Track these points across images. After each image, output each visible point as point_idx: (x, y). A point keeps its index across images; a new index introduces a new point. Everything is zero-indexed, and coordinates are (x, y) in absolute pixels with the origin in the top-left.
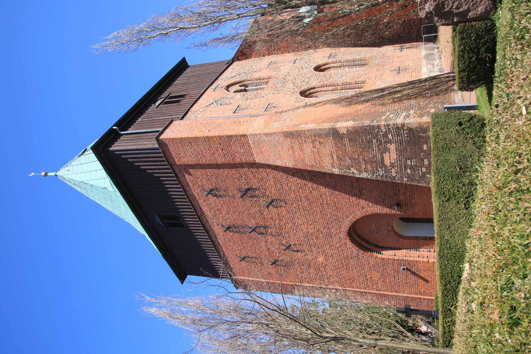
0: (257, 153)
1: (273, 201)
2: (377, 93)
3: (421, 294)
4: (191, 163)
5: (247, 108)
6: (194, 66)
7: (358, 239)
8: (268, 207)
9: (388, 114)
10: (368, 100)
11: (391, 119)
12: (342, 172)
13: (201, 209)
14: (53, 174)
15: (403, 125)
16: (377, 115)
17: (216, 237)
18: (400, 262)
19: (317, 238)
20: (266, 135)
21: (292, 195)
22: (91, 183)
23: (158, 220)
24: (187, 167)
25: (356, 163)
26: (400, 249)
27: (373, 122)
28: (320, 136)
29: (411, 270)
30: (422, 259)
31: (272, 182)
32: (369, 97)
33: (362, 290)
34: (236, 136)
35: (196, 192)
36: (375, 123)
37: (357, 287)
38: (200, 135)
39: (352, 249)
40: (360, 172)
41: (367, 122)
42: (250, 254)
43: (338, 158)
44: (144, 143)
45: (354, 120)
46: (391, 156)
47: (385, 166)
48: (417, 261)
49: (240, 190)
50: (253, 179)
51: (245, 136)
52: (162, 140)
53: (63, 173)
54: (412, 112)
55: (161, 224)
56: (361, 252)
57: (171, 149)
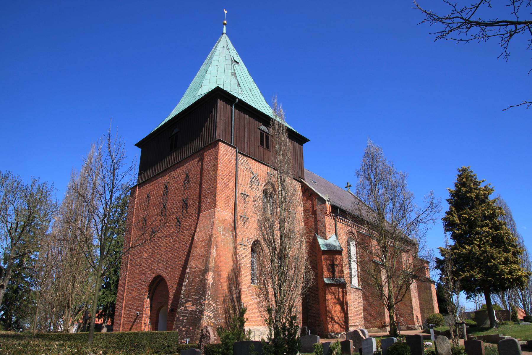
0: (205, 214)
1: (180, 222)
2: (237, 297)
3: (123, 325)
4: (205, 164)
5: (245, 202)
6: (301, 150)
7: (156, 282)
8: (176, 218)
9: (215, 305)
10: (231, 292)
11: (209, 307)
12: (187, 274)
13: (179, 167)
14: (225, 31)
15: (203, 315)
16: (214, 298)
17: (162, 177)
18: (142, 311)
19: (158, 253)
20: (213, 222)
21: (182, 237)
22: (209, 70)
23: (176, 130)
24: (202, 160)
25: (189, 285)
26: (151, 311)
27: (209, 295)
28: (207, 260)
29: (137, 319)
30: (143, 326)
31: (190, 223)
32: (234, 292)
33: (126, 284)
34: (215, 200)
35: (188, 165)
36: (207, 297)
37: (128, 280)
38: (219, 173)
39: (150, 277)
41: (209, 292)
42: (151, 202)
43: (194, 271)
44: (222, 126)
45: (213, 283)
46: (190, 307)
47: (186, 303)
48: (141, 323)
49: (187, 199)
50: (192, 210)
51: (215, 206)
52: (218, 144)
53: (225, 40)
54: (213, 320)
55: (173, 133)
56: (148, 284)
57: (212, 150)
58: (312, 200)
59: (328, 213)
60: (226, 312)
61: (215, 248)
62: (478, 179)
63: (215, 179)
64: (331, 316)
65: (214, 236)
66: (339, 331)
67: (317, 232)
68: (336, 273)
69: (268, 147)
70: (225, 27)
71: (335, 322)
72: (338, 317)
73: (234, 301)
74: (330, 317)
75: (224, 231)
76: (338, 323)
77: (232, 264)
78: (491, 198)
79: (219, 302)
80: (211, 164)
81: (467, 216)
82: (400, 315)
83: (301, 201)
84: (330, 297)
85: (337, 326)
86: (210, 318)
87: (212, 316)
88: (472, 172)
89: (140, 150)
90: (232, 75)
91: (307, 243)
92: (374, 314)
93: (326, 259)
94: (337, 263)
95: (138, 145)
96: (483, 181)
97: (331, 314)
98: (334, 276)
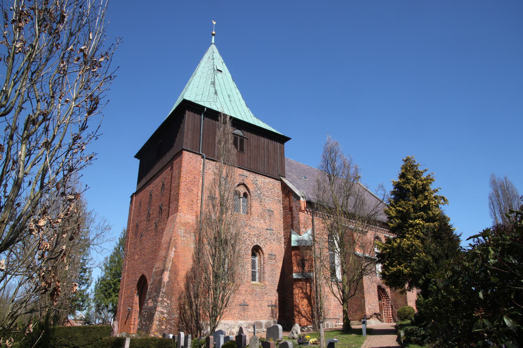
14: (213, 41)
16: (169, 295)
18: (132, 307)
23: (161, 141)
27: (163, 293)
33: (124, 283)
36: (161, 294)
40: (151, 285)
45: (168, 282)
51: (177, 211)
52: (182, 152)
53: (213, 48)
54: (166, 316)
56: (136, 282)
57: (179, 159)
58: (289, 198)
59: (303, 208)
60: (181, 308)
61: (174, 249)
62: (420, 169)
63: (178, 186)
64: (298, 310)
65: (173, 239)
66: (305, 324)
67: (292, 228)
68: (306, 268)
69: (242, 149)
70: (213, 37)
71: (302, 316)
72: (305, 311)
73: (191, 297)
74: (297, 311)
75: (185, 233)
76: (305, 317)
77: (192, 264)
78: (432, 187)
79: (174, 299)
80: (177, 172)
81: (401, 209)
82: (395, 307)
83: (281, 198)
84: (297, 292)
85: (304, 319)
86: (162, 313)
87: (165, 311)
88: (414, 162)
89: (139, 160)
90: (211, 84)
91: (285, 239)
92: (355, 307)
93: (296, 255)
94: (308, 257)
95: (136, 157)
96: (426, 170)
97: (299, 308)
98: (303, 272)
